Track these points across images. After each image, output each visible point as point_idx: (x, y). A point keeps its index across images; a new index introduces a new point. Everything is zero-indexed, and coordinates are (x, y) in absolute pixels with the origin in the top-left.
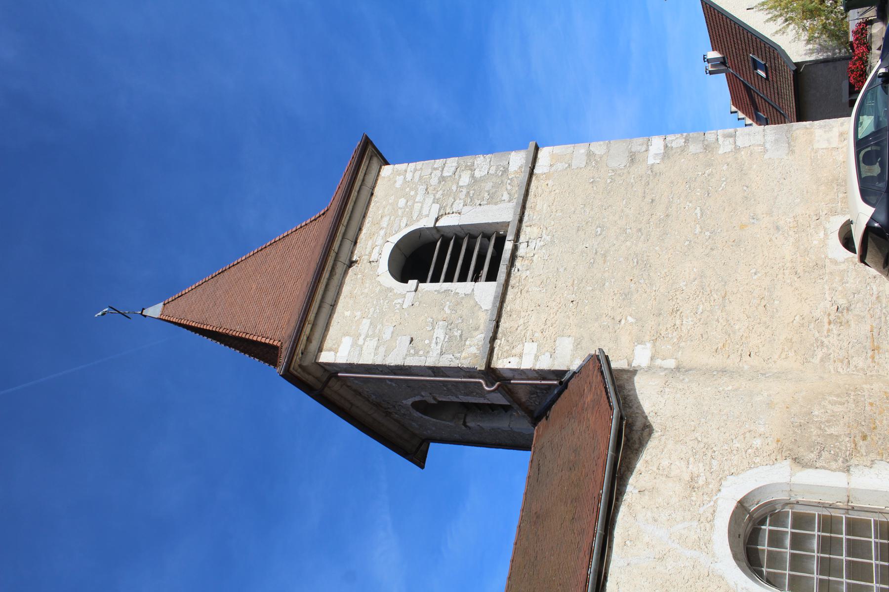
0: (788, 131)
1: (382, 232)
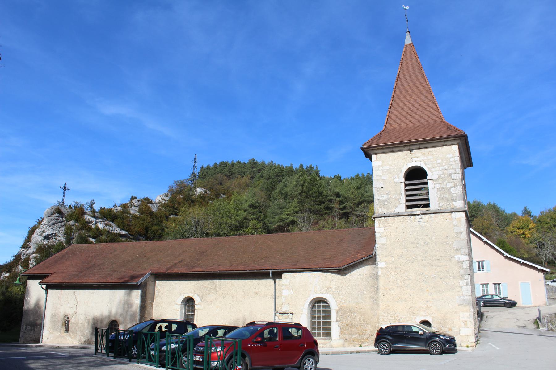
1: (425, 158)
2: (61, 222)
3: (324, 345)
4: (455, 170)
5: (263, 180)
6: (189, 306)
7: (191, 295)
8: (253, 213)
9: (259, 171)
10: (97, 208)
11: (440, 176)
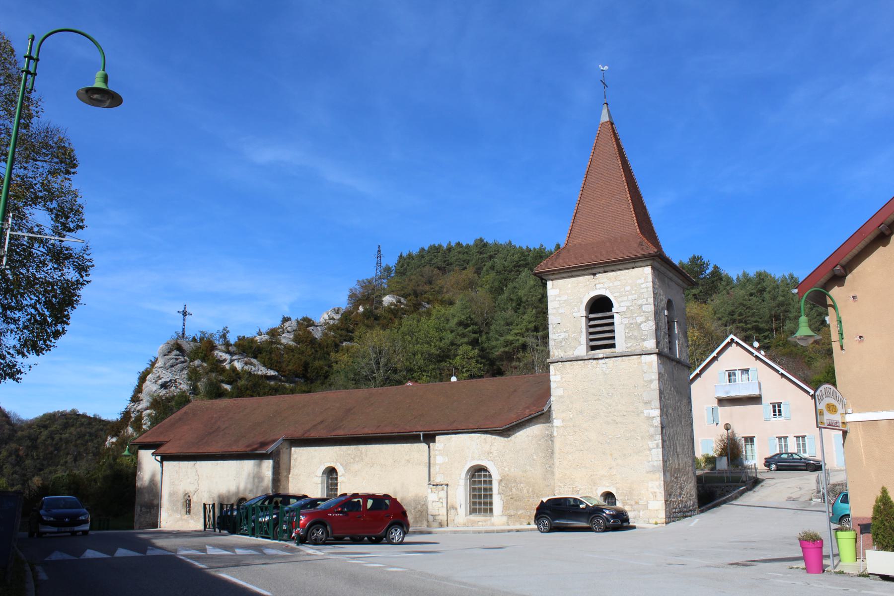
0: (653, 471)
2: (183, 362)
5: (493, 274)
6: (332, 479)
7: (333, 465)
8: (463, 335)
9: (491, 257)
10: (232, 339)
11: (628, 307)
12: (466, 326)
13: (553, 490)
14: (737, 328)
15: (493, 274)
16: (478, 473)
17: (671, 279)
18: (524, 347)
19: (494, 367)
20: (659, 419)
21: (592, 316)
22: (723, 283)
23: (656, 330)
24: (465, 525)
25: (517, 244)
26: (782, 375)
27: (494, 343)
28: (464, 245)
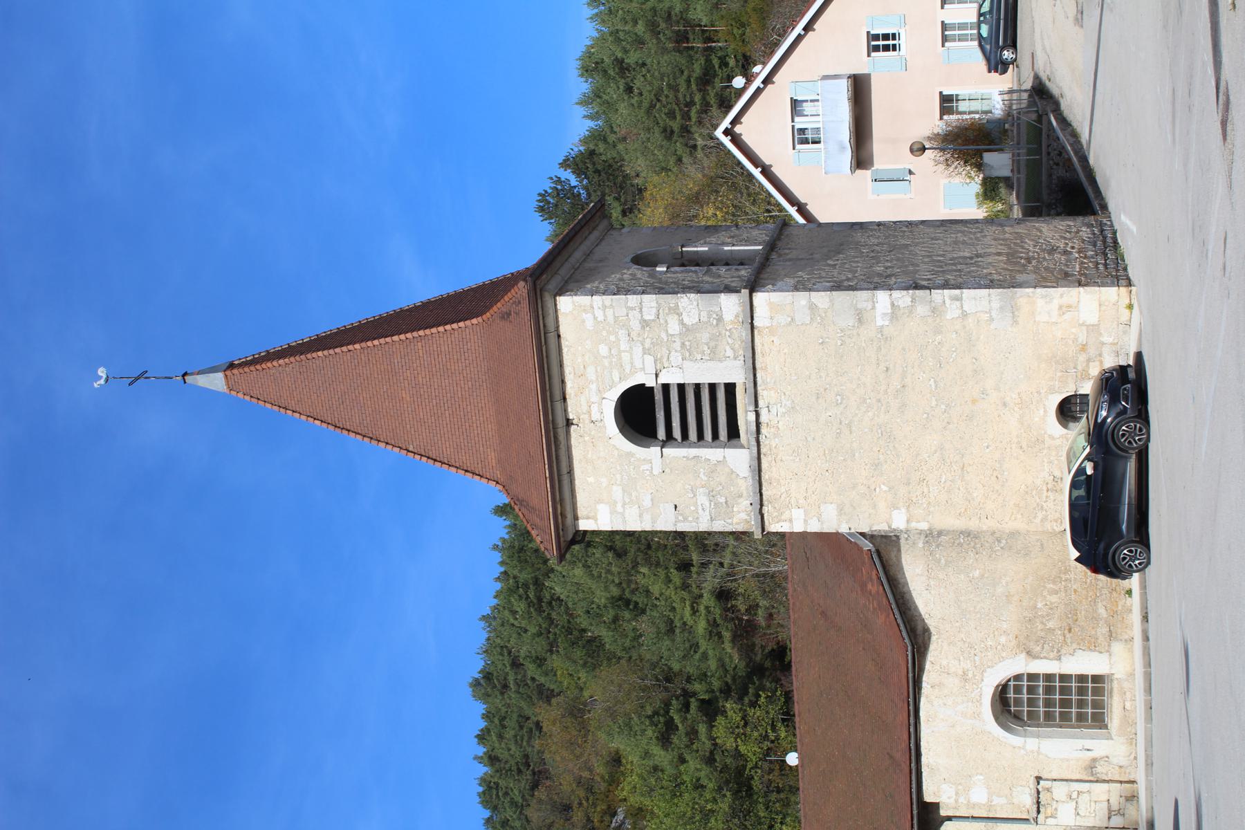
1: (593, 387)
3: (1128, 695)
4: (632, 309)
5: (556, 662)
8: (693, 734)
9: (516, 664)
11: (646, 352)
12: (670, 726)
13: (1054, 534)
14: (700, 122)
15: (556, 662)
16: (1010, 705)
17: (588, 255)
18: (723, 595)
19: (769, 669)
20: (897, 294)
21: (661, 434)
22: (601, 147)
23: (699, 291)
24: (1132, 741)
25: (488, 603)
26: (807, 28)
27: (713, 664)
28: (482, 724)
